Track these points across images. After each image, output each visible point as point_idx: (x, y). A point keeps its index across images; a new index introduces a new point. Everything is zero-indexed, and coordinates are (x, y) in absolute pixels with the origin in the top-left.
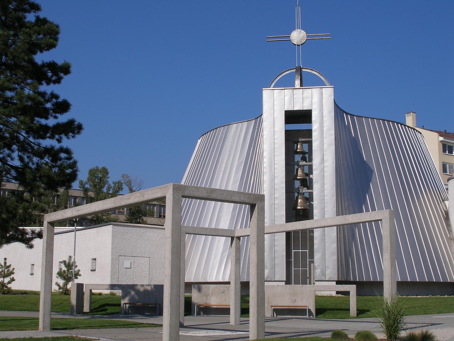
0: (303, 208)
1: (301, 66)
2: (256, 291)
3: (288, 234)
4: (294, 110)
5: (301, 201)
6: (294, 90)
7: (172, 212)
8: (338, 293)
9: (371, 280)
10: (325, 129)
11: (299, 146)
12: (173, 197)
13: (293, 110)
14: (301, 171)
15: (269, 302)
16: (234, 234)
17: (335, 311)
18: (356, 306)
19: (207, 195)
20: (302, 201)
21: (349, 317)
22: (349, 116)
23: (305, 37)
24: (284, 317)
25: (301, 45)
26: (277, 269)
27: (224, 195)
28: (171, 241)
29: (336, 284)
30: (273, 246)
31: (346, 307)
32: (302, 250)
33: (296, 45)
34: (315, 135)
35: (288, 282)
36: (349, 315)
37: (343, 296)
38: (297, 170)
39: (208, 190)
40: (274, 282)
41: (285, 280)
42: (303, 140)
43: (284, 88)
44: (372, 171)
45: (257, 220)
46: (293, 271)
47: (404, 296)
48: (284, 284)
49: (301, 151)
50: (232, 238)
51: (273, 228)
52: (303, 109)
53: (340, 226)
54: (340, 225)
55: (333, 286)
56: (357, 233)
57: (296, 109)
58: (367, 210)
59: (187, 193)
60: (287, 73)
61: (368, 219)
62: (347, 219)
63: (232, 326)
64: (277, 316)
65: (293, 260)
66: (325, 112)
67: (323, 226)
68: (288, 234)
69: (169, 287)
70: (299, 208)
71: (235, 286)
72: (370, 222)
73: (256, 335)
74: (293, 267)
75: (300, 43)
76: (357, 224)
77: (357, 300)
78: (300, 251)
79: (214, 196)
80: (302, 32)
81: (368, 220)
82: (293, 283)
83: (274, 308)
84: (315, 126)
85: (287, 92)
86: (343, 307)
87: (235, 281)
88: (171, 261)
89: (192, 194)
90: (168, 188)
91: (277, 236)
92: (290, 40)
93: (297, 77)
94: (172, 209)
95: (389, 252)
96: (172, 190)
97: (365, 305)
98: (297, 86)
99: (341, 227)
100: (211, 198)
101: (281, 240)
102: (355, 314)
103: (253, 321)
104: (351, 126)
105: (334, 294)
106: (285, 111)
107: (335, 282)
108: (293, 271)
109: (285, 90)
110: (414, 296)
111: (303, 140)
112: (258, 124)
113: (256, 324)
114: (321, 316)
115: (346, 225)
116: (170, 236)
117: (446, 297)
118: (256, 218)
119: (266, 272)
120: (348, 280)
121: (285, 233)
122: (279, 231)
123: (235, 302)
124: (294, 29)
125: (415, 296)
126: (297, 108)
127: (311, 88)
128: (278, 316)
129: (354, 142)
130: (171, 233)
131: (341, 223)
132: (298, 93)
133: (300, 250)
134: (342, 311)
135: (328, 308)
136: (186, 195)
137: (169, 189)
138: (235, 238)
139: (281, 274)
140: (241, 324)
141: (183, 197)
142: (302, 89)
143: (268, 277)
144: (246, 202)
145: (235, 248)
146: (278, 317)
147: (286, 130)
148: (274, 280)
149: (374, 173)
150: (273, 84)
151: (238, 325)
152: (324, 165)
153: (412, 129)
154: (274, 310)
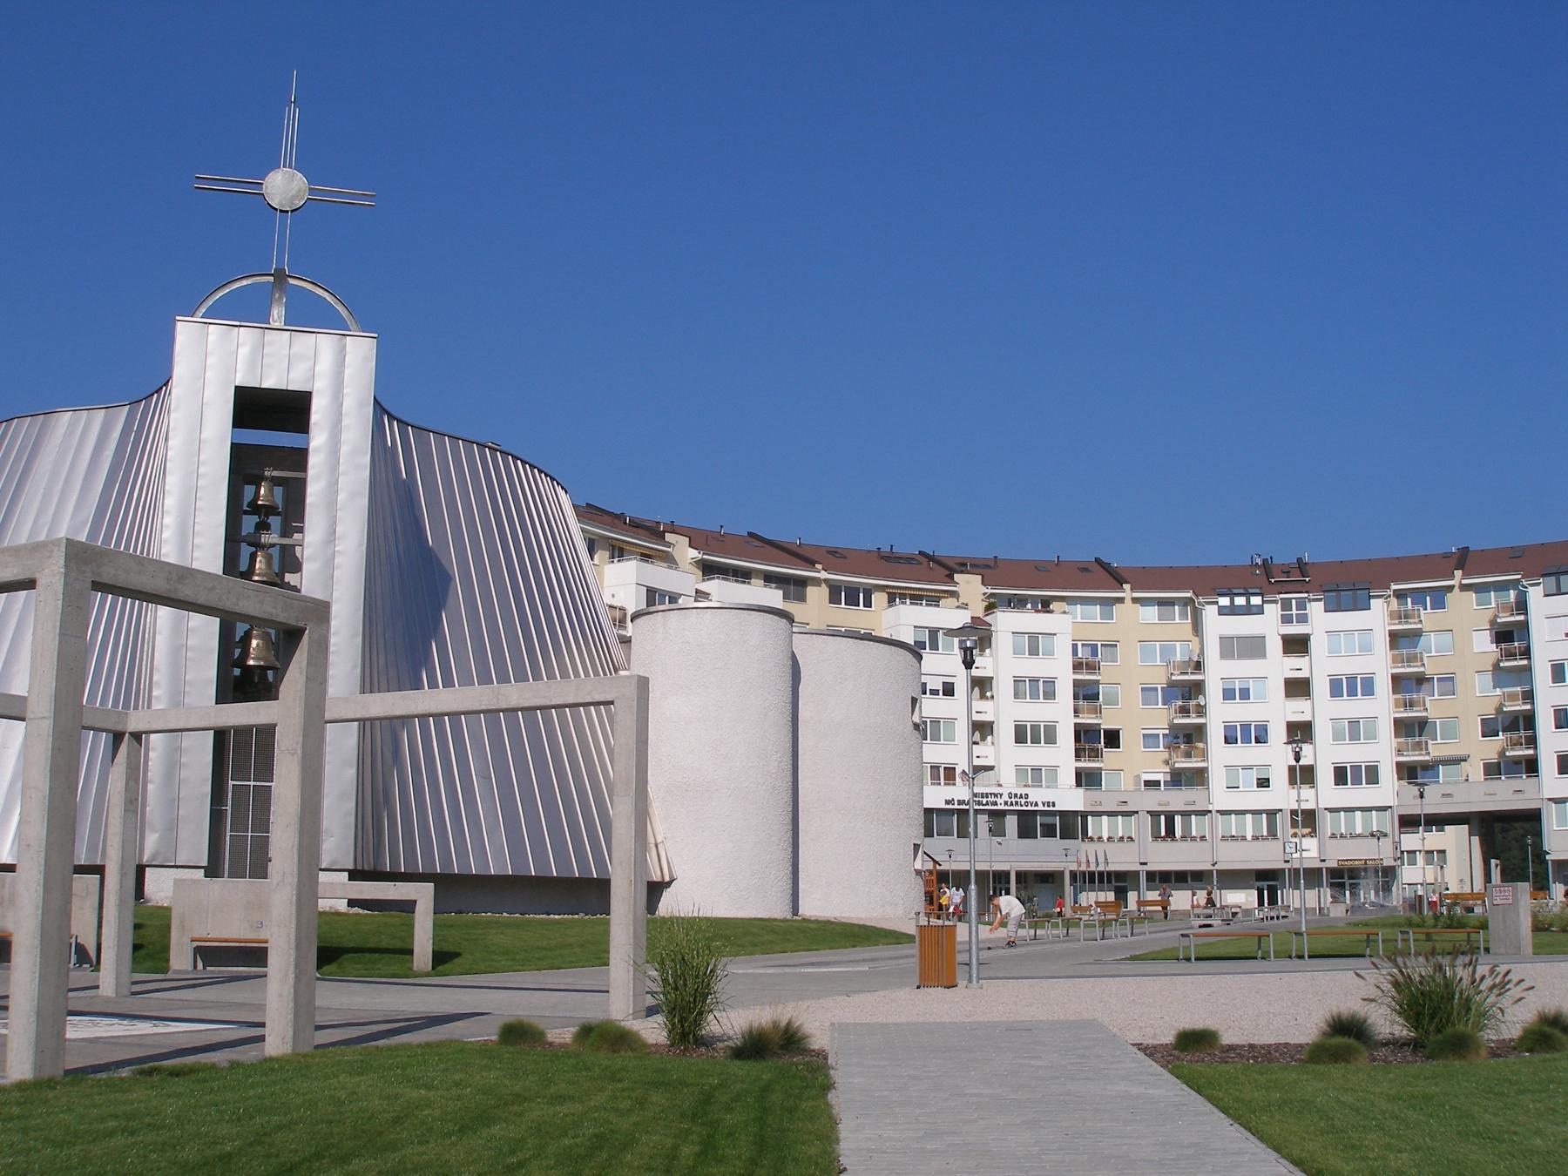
0: (262, 663)
1: (286, 268)
2: (294, 902)
3: (220, 735)
4: (263, 386)
5: (258, 645)
6: (266, 331)
7: (60, 634)
8: (351, 903)
9: (419, 870)
10: (344, 449)
11: (262, 489)
12: (66, 585)
13: (258, 386)
14: (263, 560)
15: (183, 926)
16: (126, 724)
17: (367, 955)
18: (431, 941)
19: (168, 587)
20: (261, 645)
21: (409, 973)
22: (395, 423)
23: (305, 190)
24: (236, 972)
25: (292, 211)
26: (184, 833)
27: (217, 591)
28: (51, 731)
29: (349, 880)
30: (173, 765)
31: (408, 947)
32: (258, 781)
33: (276, 209)
34: (315, 461)
35: (213, 870)
36: (409, 965)
37: (366, 912)
38: (253, 557)
39: (170, 573)
40: (172, 869)
41: (205, 864)
42: (275, 473)
43: (238, 323)
44: (448, 578)
45: (307, 677)
46: (228, 838)
47: (517, 915)
48: (203, 874)
49: (267, 503)
50: (118, 737)
51: (258, 713)
52: (289, 389)
53: (373, 722)
54: (372, 720)
55: (194, 881)
56: (404, 740)
57: (268, 384)
58: (433, 685)
59: (107, 576)
60: (244, 282)
61: (434, 709)
62: (504, 695)
63: (108, 1000)
64: (204, 968)
65: (229, 808)
66: (349, 403)
67: (424, 712)
68: (220, 735)
69: (39, 884)
70: (251, 662)
71: (121, 880)
72: (438, 717)
73: (291, 1040)
74: (228, 828)
75: (290, 207)
76: (406, 720)
77: (435, 925)
78: (252, 783)
79: (186, 592)
80: (298, 177)
81: (571, 700)
82: (226, 875)
83: (197, 946)
84: (318, 440)
85: (246, 336)
86: (383, 943)
87: (122, 866)
88: (47, 798)
89: (122, 580)
90: (48, 555)
91: (188, 740)
92: (263, 194)
93: (277, 295)
94: (58, 624)
95: (632, 794)
96: (62, 562)
97: (442, 938)
98: (276, 321)
99: (368, 723)
100: (178, 598)
101: (201, 751)
102: (428, 963)
103: (280, 996)
104: (398, 452)
105: (342, 906)
106: (236, 387)
107: (347, 873)
108: (228, 838)
109: (241, 328)
110: (542, 916)
111: (275, 473)
112: (138, 418)
113: (292, 1004)
114: (332, 968)
115: (378, 722)
116: (47, 715)
117: (517, 917)
118: (305, 673)
119: (152, 841)
120: (379, 869)
121: (213, 731)
122: (166, 728)
123: (119, 929)
124: (276, 166)
125: (544, 916)
126: (270, 382)
127: (314, 332)
128: (208, 968)
129: (407, 493)
130: (51, 702)
131: (368, 716)
132: (279, 342)
133: (250, 781)
134: (386, 956)
135: (345, 945)
136: (106, 582)
137: (50, 557)
138: (127, 734)
139: (195, 846)
140: (133, 994)
141: (98, 586)
142: (289, 332)
143: (154, 856)
144: (278, 620)
145: (125, 765)
146: (210, 971)
147: (234, 441)
148: (173, 864)
149: (453, 583)
150: (203, 310)
151: (126, 996)
152: (336, 549)
153: (548, 478)
154: (197, 950)
